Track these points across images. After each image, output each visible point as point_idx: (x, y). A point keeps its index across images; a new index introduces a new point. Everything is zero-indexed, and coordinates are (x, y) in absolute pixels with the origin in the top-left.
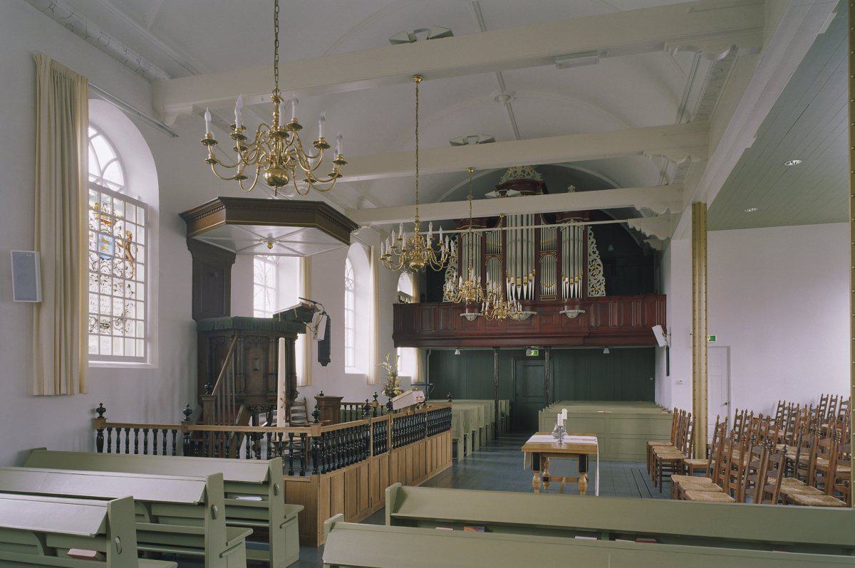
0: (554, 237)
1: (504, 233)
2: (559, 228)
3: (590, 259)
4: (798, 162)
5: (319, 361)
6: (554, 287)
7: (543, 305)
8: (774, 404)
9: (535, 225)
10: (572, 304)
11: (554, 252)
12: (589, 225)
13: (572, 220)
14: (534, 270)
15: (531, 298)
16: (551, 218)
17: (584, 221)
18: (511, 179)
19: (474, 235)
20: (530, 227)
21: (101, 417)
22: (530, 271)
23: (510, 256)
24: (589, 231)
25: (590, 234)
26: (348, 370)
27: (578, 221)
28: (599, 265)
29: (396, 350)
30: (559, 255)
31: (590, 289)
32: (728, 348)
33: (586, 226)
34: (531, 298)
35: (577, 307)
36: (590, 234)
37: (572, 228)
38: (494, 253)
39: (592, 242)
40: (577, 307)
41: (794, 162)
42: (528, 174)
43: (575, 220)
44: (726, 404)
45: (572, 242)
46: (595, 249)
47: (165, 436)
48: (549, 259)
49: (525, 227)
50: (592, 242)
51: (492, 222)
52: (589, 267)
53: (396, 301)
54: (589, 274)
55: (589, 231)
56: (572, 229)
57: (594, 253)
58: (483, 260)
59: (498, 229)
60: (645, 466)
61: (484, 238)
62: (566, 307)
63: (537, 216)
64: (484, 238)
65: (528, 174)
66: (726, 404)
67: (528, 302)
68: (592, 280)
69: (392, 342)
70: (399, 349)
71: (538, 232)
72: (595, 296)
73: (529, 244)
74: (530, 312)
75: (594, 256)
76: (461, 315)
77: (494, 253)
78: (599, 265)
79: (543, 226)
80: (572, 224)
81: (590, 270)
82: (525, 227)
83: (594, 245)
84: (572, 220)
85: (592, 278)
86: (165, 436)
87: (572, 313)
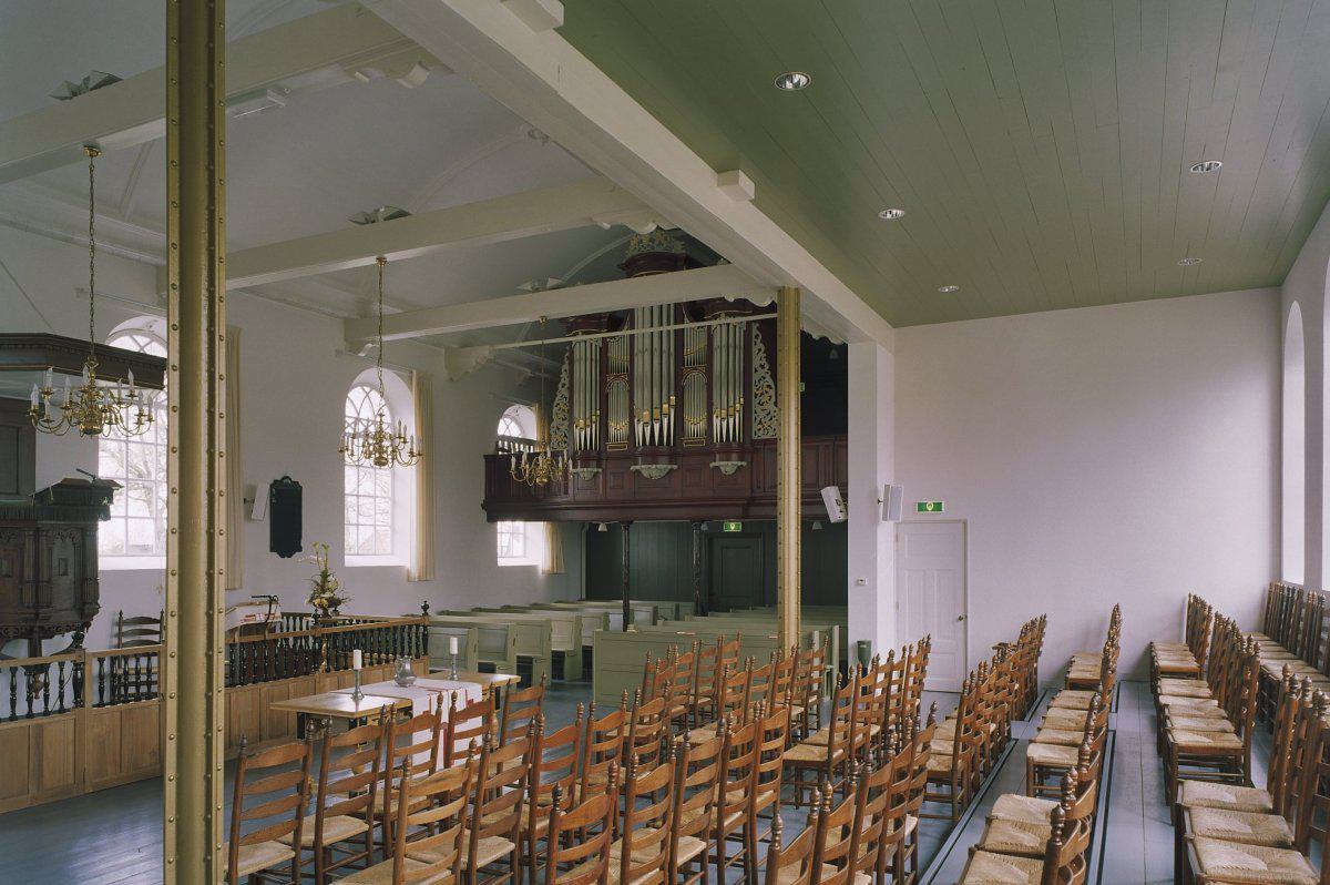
0: (703, 343)
1: (632, 336)
2: (709, 327)
3: (756, 377)
4: (899, 212)
5: (283, 556)
6: (702, 425)
7: (610, 457)
8: (1184, 602)
9: (676, 323)
10: (726, 450)
11: (702, 368)
12: (755, 321)
13: (723, 315)
14: (673, 398)
15: (591, 448)
16: (697, 310)
17: (744, 315)
18: (636, 252)
19: (588, 345)
20: (665, 328)
21: (426, 614)
22: (664, 400)
23: (718, 373)
24: (755, 332)
25: (757, 337)
26: (502, 562)
27: (734, 315)
28: (769, 386)
29: (495, 533)
30: (709, 373)
31: (755, 427)
32: (965, 523)
33: (749, 324)
34: (591, 448)
35: (734, 456)
36: (757, 337)
37: (724, 328)
38: (618, 372)
39: (760, 350)
40: (734, 456)
41: (894, 212)
42: (660, 244)
43: (727, 315)
44: (960, 619)
45: (731, 350)
46: (764, 361)
47: (61, 670)
48: (695, 378)
49: (656, 329)
50: (760, 350)
51: (616, 320)
52: (754, 390)
53: (491, 451)
54: (755, 402)
55: (755, 332)
56: (755, 326)
57: (762, 367)
58: (679, 376)
59: (625, 332)
60: (75, 795)
61: (604, 348)
62: (717, 456)
63: (677, 306)
64: (604, 348)
65: (660, 244)
66: (960, 619)
67: (662, 449)
68: (759, 411)
69: (484, 515)
70: (503, 527)
71: (679, 334)
72: (763, 437)
73: (664, 355)
74: (669, 467)
75: (762, 372)
76: (712, 465)
77: (618, 372)
78: (769, 386)
79: (687, 325)
80: (723, 320)
81: (756, 394)
82: (656, 329)
83: (762, 355)
84: (723, 315)
85: (759, 409)
86: (61, 670)
87: (728, 467)
